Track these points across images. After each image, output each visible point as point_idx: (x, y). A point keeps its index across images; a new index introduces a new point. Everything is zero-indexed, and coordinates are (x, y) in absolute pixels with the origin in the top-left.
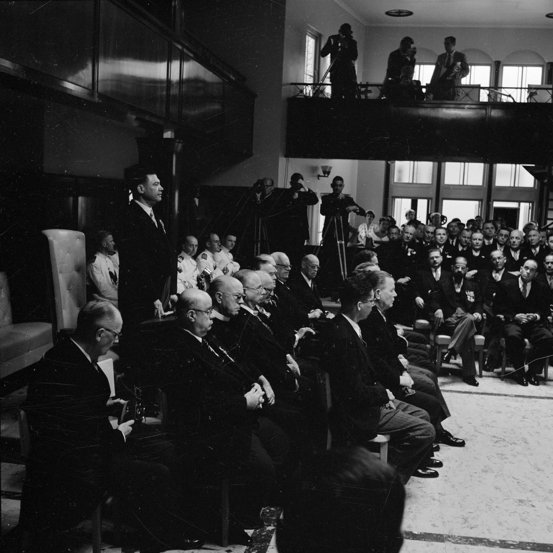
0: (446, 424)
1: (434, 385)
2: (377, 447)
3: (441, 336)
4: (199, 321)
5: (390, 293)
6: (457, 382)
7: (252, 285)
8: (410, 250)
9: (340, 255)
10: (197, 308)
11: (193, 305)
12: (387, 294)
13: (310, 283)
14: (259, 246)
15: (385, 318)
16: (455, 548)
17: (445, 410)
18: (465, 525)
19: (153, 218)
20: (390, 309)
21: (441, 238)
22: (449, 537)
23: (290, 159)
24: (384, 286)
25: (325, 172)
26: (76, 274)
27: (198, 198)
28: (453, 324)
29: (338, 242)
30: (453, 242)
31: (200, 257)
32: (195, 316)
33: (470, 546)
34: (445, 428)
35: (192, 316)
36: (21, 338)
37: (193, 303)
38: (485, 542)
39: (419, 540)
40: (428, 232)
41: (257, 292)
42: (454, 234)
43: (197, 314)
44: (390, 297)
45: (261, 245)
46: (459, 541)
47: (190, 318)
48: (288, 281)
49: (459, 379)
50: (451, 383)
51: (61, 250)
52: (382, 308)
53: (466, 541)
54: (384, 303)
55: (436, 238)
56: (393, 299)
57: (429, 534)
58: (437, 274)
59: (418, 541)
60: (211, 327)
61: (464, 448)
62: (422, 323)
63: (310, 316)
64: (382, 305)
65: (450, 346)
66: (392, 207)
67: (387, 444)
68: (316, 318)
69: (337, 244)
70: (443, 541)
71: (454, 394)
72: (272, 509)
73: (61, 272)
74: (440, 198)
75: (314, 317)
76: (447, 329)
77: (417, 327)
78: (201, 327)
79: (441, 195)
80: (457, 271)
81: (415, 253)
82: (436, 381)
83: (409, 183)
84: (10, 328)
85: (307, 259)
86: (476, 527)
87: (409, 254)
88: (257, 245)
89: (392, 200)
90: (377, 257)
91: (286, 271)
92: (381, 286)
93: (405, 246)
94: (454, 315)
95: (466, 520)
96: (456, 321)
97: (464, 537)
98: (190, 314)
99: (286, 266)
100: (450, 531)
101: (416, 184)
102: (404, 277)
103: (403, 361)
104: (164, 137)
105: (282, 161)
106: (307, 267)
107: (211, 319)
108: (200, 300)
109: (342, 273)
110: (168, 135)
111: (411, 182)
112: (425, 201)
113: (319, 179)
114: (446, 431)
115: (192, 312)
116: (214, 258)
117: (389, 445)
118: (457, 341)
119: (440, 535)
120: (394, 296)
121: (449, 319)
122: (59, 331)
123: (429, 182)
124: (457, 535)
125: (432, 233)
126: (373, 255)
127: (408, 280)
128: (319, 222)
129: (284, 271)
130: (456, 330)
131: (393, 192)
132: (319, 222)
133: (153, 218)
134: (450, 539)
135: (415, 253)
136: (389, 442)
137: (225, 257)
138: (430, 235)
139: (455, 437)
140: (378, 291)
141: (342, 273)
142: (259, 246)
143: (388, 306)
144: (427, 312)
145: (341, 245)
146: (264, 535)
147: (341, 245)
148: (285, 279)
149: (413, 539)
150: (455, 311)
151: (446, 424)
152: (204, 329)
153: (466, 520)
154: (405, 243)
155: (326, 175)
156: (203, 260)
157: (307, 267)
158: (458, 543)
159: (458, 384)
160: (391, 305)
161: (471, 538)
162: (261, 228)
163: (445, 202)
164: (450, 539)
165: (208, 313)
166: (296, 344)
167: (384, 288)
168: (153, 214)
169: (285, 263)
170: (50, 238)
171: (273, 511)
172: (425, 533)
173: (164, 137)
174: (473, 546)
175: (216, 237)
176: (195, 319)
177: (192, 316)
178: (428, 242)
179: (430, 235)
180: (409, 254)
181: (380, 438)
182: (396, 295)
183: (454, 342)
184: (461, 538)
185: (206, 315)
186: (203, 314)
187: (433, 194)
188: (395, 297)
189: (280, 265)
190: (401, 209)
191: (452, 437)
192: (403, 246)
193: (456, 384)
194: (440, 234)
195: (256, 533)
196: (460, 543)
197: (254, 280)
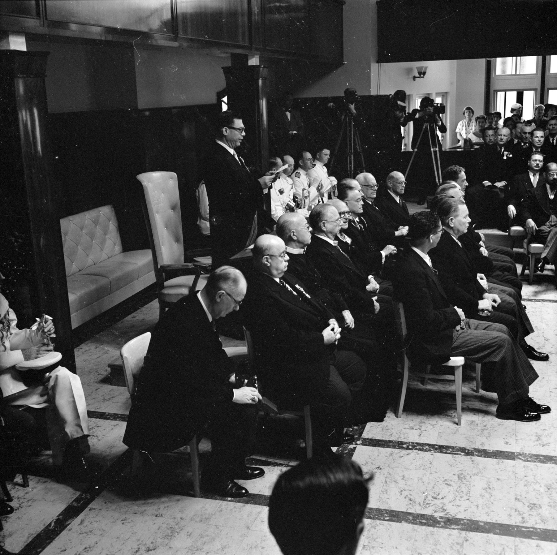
0: (529, 340)
1: (515, 304)
2: (452, 370)
3: (533, 245)
4: (274, 264)
5: (464, 220)
6: (550, 290)
7: (330, 218)
8: (506, 153)
9: (434, 162)
10: (270, 253)
11: (267, 251)
12: (460, 221)
13: (397, 199)
14: (352, 158)
15: (460, 244)
16: (524, 466)
17: (528, 327)
18: (537, 442)
19: (236, 157)
20: (464, 234)
21: (540, 141)
22: (520, 454)
23: (382, 64)
24: (457, 213)
25: (420, 73)
26: (171, 212)
27: (290, 112)
28: (546, 232)
29: (432, 150)
30: (553, 140)
31: (294, 175)
32: (269, 260)
33: (539, 464)
34: (528, 343)
35: (267, 261)
36: (130, 268)
37: (266, 249)
38: (554, 460)
39: (490, 457)
40: (525, 133)
41: (335, 224)
42: (554, 132)
43: (271, 259)
44: (464, 223)
45: (354, 157)
46: (529, 459)
47: (266, 263)
48: (376, 200)
49: (553, 287)
50: (543, 291)
51: (156, 192)
52: (456, 234)
53: (536, 459)
54: (458, 231)
55: (533, 140)
56: (468, 225)
57: (501, 452)
58: (534, 179)
59: (489, 459)
60: (286, 268)
61: (548, 362)
62: (517, 230)
63: (397, 233)
64: (456, 232)
65: (543, 256)
66: (494, 99)
67: (461, 368)
68: (403, 235)
69: (431, 151)
70: (513, 459)
71: (546, 303)
72: (355, 427)
73: (157, 212)
74: (546, 89)
75: (400, 234)
76: (540, 237)
77: (511, 234)
78: (277, 269)
79: (547, 85)
80: (551, 178)
81: (511, 156)
82: (518, 297)
83: (512, 75)
84: (120, 257)
85: (393, 177)
86: (548, 444)
87: (505, 158)
88: (350, 157)
89: (494, 94)
90: (465, 172)
91: (373, 191)
92: (455, 214)
93: (501, 149)
94: (548, 223)
95: (539, 438)
96: (549, 229)
97: (535, 455)
98: (265, 259)
99: (373, 186)
100: (522, 448)
101: (520, 75)
102: (500, 181)
103: (484, 283)
104: (249, 64)
105: (374, 66)
106: (394, 185)
107: (285, 261)
108: (272, 246)
109: (437, 181)
110: (254, 61)
111: (514, 73)
112: (532, 93)
113: (414, 80)
114: (529, 346)
115: (267, 258)
116: (308, 175)
117: (463, 368)
118: (550, 250)
119: (511, 452)
120: (468, 221)
121: (543, 228)
122: (159, 267)
123: (534, 72)
124: (528, 453)
125: (529, 133)
126: (460, 171)
127: (504, 184)
128: (408, 132)
129: (370, 191)
130: (549, 239)
131: (495, 85)
132: (408, 132)
133: (236, 157)
134: (521, 457)
135: (511, 156)
136: (464, 366)
137: (320, 171)
138: (527, 135)
139: (538, 351)
140: (452, 219)
141: (437, 181)
142: (352, 158)
143: (463, 232)
144: (520, 220)
145: (435, 152)
146: (346, 453)
147: (435, 152)
148: (372, 198)
149: (485, 457)
150: (549, 219)
151: (529, 340)
152: (280, 272)
153: (539, 438)
154: (501, 146)
155: (422, 76)
156: (297, 179)
157: (394, 185)
158: (528, 461)
159: (551, 292)
160: (466, 231)
161: (542, 456)
162: (354, 139)
163: (551, 92)
164: (521, 457)
165: (282, 257)
166: (383, 260)
167: (456, 216)
168: (235, 153)
169: (371, 184)
170: (145, 183)
171: (356, 430)
172: (497, 451)
173: (249, 64)
174: (542, 464)
175: (308, 155)
176: (270, 263)
177: (267, 261)
178: (527, 143)
179: (527, 135)
180: (505, 158)
181: (458, 361)
182: (470, 220)
183: (547, 251)
184: (532, 456)
185: (280, 258)
186: (277, 258)
187: (537, 84)
188: (469, 223)
189: (366, 186)
190: (505, 103)
191: (536, 352)
192: (499, 149)
193: (549, 292)
194: (537, 137)
195: (339, 451)
196: (530, 461)
197: (332, 213)
